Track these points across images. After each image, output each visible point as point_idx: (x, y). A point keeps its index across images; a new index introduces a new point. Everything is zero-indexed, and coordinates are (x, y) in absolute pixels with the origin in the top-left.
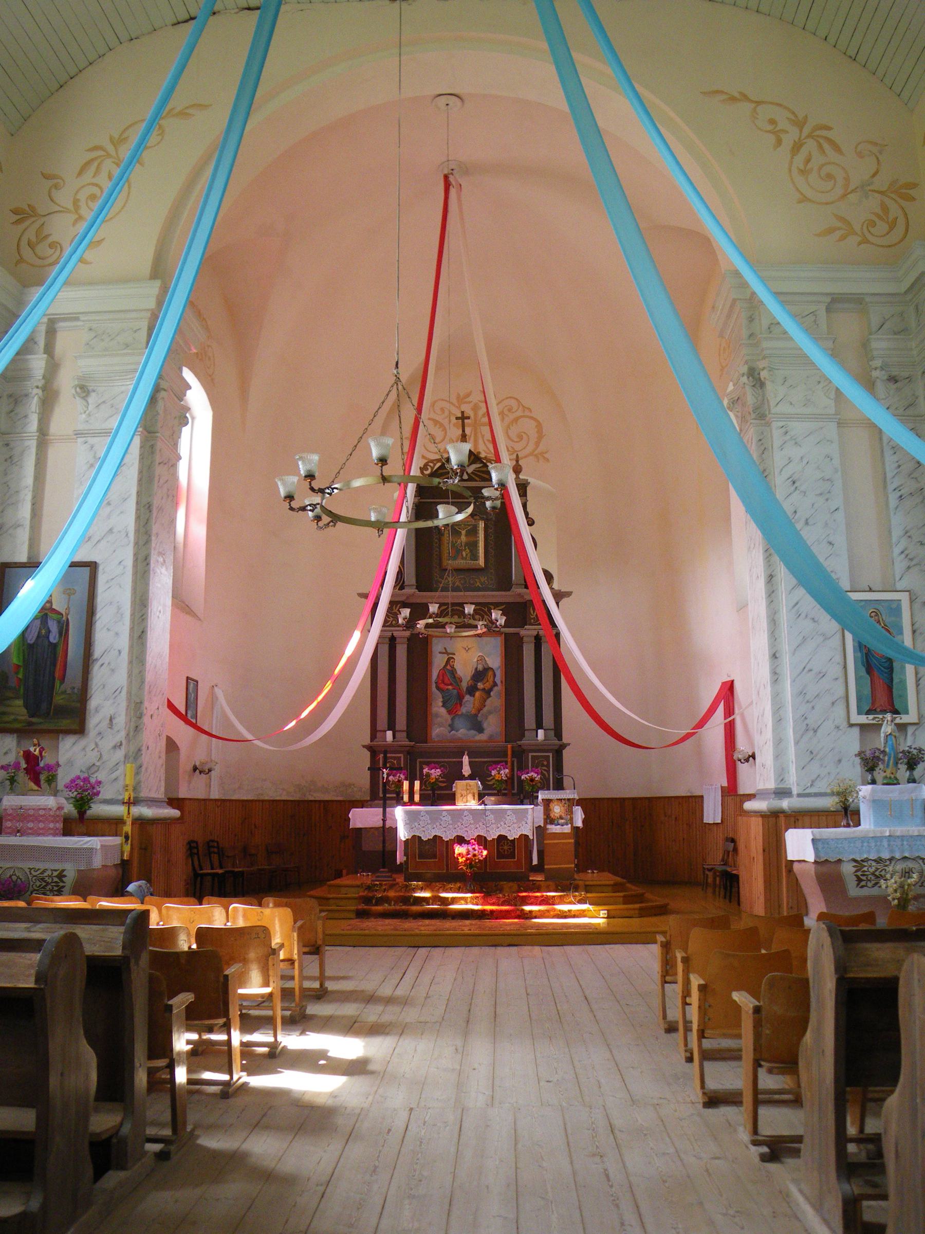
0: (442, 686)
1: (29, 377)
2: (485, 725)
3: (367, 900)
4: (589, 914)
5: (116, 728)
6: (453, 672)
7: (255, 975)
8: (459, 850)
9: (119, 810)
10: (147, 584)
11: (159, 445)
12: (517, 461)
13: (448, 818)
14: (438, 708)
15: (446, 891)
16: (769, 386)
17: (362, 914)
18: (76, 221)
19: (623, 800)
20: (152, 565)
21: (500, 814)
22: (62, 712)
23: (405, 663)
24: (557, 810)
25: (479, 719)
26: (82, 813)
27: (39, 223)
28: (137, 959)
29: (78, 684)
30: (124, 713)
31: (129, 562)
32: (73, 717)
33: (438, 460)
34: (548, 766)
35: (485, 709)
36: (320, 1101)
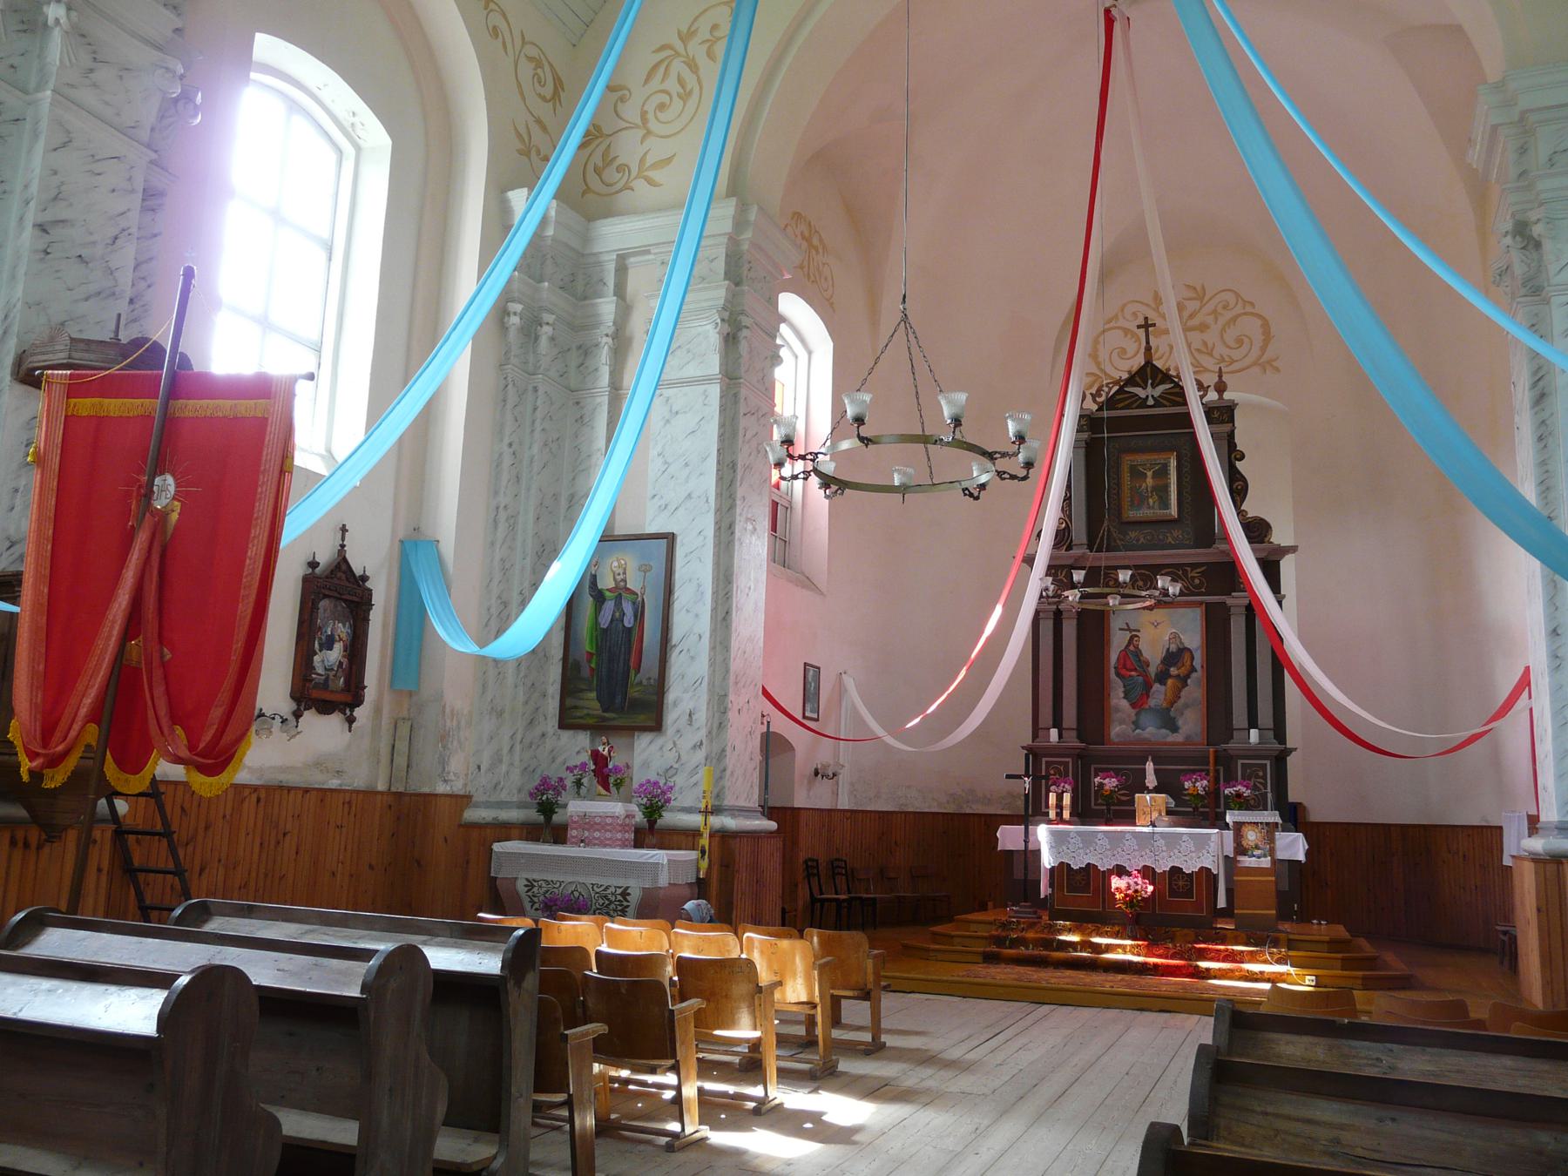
0: (1123, 672)
1: (596, 325)
2: (1180, 723)
3: (999, 941)
4: (1289, 979)
5: (696, 725)
6: (1138, 653)
7: (745, 1018)
8: (1116, 882)
9: (695, 820)
10: (731, 557)
11: (743, 392)
12: (1220, 376)
13: (1105, 843)
14: (1118, 700)
15: (1101, 935)
16: (1548, 246)
17: (990, 958)
18: (644, 138)
19: (1387, 828)
20: (737, 534)
21: (1172, 840)
22: (637, 706)
23: (1075, 647)
24: (1251, 836)
25: (1172, 714)
26: (652, 823)
27: (603, 147)
28: (519, 983)
29: (655, 674)
30: (704, 708)
31: (710, 532)
32: (647, 711)
33: (1116, 383)
34: (1264, 777)
35: (1182, 701)
36: (768, 1167)
